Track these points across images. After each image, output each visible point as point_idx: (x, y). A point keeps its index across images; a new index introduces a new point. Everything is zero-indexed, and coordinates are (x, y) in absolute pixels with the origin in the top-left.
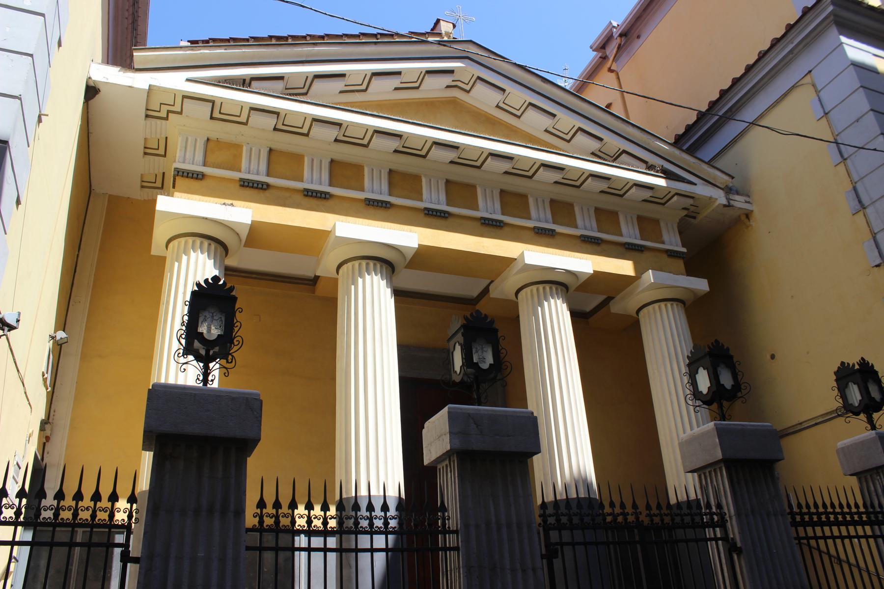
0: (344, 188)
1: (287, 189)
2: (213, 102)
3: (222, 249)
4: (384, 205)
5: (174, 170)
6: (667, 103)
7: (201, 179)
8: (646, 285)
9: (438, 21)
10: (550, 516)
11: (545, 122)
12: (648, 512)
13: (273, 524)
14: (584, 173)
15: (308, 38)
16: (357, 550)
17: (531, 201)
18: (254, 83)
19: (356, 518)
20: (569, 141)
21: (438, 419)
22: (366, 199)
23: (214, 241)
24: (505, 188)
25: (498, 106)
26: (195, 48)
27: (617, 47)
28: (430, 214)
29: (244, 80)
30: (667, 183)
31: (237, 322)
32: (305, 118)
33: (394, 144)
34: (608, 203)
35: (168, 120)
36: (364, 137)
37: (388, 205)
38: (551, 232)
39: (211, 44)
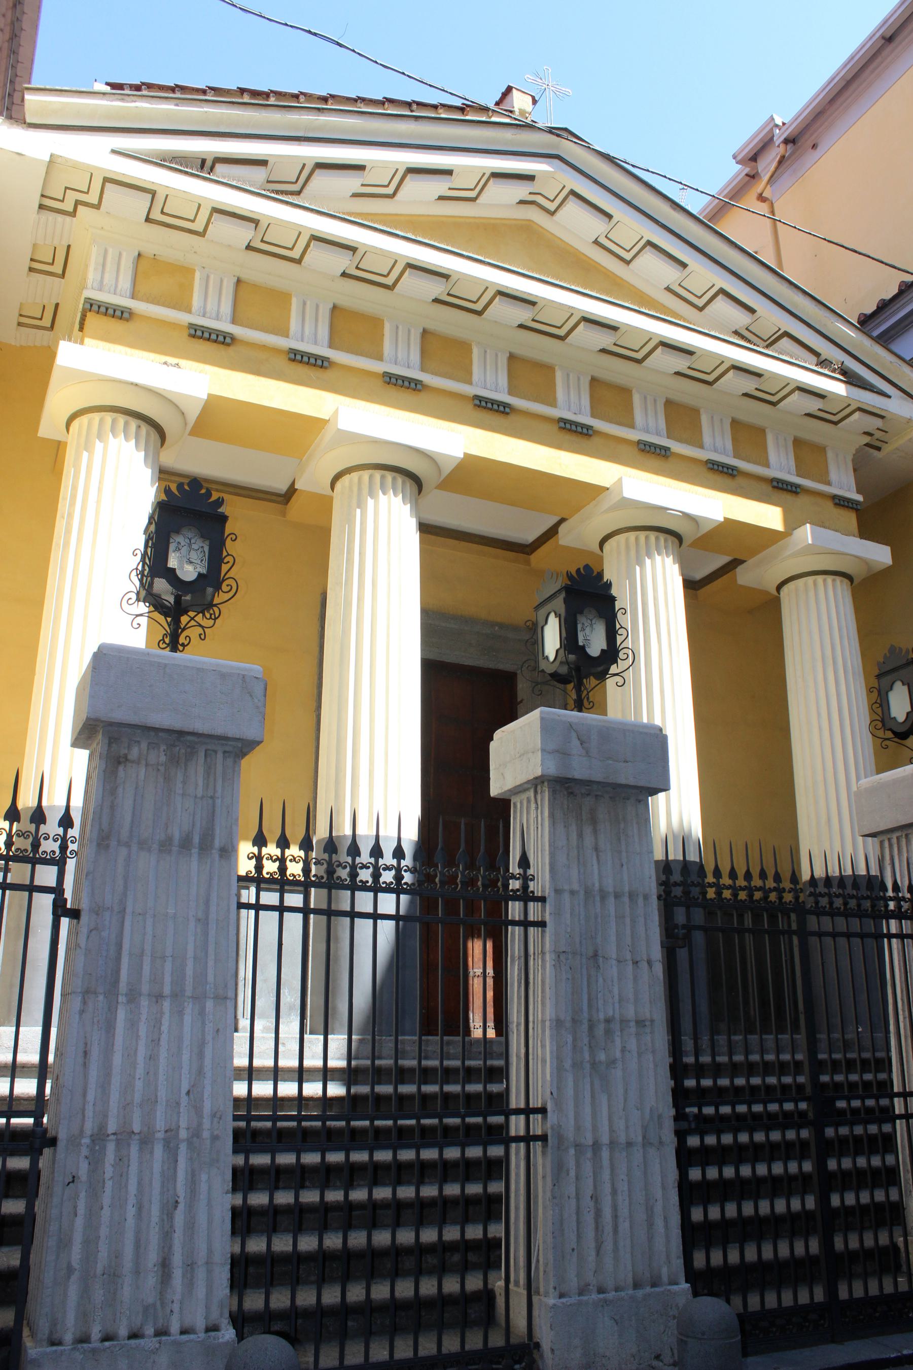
0: (352, 353)
1: (264, 347)
2: (153, 193)
3: (157, 436)
4: (413, 385)
5: (85, 302)
6: (886, 264)
7: (127, 320)
8: (800, 547)
9: (509, 89)
10: (676, 884)
11: (669, 274)
12: (812, 890)
13: (277, 871)
14: (723, 362)
15: (302, 98)
16: (353, 915)
17: (637, 399)
18: (219, 167)
19: (354, 867)
20: (701, 309)
21: (521, 727)
22: (386, 374)
23: (147, 422)
24: (599, 374)
25: (596, 242)
26: (126, 98)
27: (778, 159)
28: (483, 407)
29: (203, 162)
30: (847, 392)
31: (228, 555)
32: (300, 233)
33: (437, 289)
34: (755, 413)
35: (75, 216)
36: (389, 274)
37: (419, 387)
38: (663, 452)
39: (145, 92)
